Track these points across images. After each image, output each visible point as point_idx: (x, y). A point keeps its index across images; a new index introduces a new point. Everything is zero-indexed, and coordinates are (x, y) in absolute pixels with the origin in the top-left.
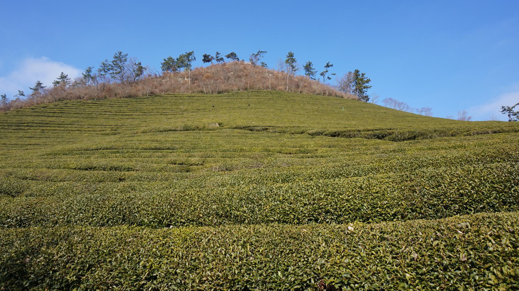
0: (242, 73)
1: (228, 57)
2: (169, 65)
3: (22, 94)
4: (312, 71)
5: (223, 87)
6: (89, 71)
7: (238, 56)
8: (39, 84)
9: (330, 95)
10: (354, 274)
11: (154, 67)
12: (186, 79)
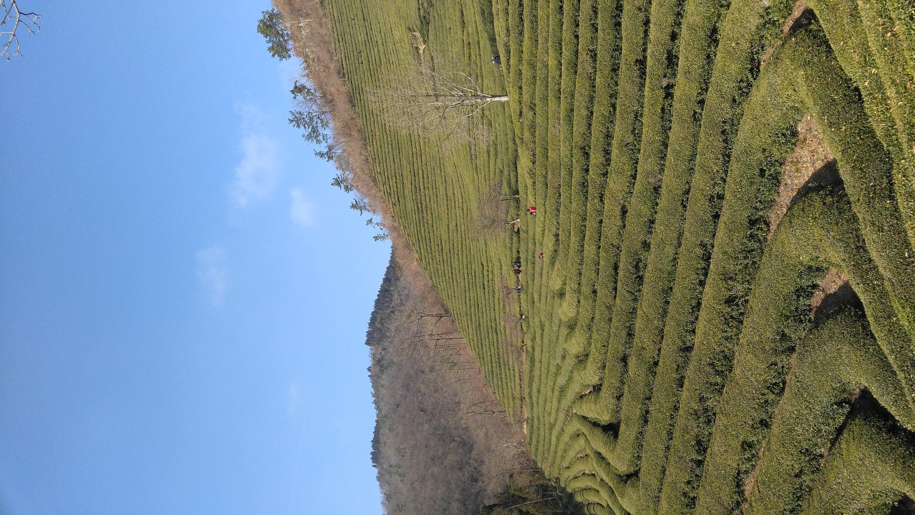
2: (279, 50)
3: (370, 221)
6: (322, 155)
8: (353, 206)
11: (292, 69)
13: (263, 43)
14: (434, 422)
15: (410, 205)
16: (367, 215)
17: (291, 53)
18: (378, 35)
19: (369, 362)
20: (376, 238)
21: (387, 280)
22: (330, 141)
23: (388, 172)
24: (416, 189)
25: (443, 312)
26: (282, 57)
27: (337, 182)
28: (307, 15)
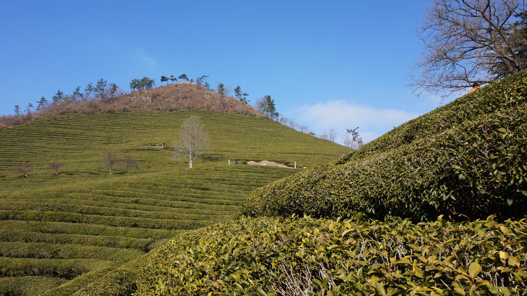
0: (188, 94)
1: (180, 78)
2: (135, 84)
3: (31, 106)
5: (173, 106)
6: (78, 89)
7: (188, 77)
8: (43, 99)
9: (246, 114)
10: (8, 125)
11: (125, 88)
12: (148, 98)
13: (140, 78)
15: (52, 130)
16: (36, 105)
17: (133, 90)
20: (17, 107)
22: (85, 96)
24: (65, 134)
26: (131, 84)
27: (59, 94)
28: (153, 101)
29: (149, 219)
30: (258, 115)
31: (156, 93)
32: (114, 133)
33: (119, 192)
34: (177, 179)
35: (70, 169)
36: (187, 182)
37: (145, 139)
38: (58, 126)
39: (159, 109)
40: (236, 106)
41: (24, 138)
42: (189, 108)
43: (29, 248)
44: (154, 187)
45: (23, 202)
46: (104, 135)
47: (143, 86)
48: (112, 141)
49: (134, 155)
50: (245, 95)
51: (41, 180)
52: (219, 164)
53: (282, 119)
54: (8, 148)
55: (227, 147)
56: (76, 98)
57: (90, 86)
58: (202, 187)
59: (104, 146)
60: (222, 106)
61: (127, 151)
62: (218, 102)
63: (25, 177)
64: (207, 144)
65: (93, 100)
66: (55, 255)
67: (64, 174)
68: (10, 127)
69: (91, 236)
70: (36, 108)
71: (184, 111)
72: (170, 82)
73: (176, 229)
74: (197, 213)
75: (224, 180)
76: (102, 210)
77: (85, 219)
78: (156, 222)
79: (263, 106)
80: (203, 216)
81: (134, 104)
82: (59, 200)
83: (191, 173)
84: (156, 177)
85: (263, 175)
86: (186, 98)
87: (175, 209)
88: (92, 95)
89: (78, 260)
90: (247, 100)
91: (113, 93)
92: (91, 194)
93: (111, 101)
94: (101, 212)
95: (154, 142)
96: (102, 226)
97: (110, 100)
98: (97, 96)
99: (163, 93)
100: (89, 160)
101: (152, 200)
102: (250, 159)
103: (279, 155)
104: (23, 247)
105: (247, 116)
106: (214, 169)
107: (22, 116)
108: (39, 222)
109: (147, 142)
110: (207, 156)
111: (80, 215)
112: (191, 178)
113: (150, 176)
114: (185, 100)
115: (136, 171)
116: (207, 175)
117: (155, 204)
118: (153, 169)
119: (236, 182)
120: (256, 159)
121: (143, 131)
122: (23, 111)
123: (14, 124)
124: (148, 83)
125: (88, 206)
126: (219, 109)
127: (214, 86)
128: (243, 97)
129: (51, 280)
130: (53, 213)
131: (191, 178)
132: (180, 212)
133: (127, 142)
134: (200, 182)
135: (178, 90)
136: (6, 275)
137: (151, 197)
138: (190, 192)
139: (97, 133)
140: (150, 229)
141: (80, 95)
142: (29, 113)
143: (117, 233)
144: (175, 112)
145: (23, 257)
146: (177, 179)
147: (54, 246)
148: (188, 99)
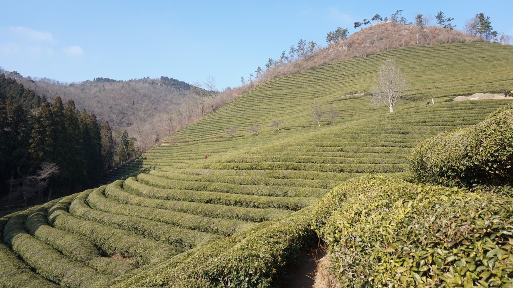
0: (384, 35)
1: (373, 19)
2: (331, 37)
3: (252, 76)
4: (443, 19)
5: (369, 50)
6: (283, 54)
7: (381, 16)
9: (453, 41)
10: (239, 94)
11: (322, 43)
12: (344, 48)
13: (334, 30)
14: (129, 109)
15: (269, 93)
16: (255, 74)
17: (329, 43)
18: (350, 80)
19: (152, 77)
20: (242, 78)
21: (183, 84)
22: (290, 58)
23: (277, 86)
24: (279, 95)
25: (214, 108)
27: (270, 61)
28: (349, 50)
29: (353, 165)
30: (468, 39)
31: (351, 41)
32: (318, 87)
33: (326, 143)
34: (377, 126)
35: (288, 125)
36: (386, 128)
37: (346, 89)
38: (273, 89)
39: (356, 57)
40: (440, 35)
41: (251, 103)
42: (386, 49)
43: (269, 189)
44: (356, 135)
45: (259, 156)
46: (310, 90)
47: (338, 37)
48: (317, 95)
49: (337, 106)
50: (449, 20)
51: (268, 136)
52: (423, 104)
53: (502, 38)
54: (242, 112)
55: (431, 84)
56: (283, 61)
57: (293, 49)
58: (402, 131)
59: (311, 101)
60: (423, 39)
61: (331, 102)
62: (418, 35)
63: (257, 135)
64: (406, 85)
65: (296, 60)
66: (285, 194)
67: (283, 130)
68: (240, 96)
69: (309, 180)
70: (256, 76)
71: (381, 53)
72: (363, 26)
73: (377, 173)
74: (397, 157)
75: (425, 122)
76: (315, 159)
77: (303, 167)
78: (359, 167)
79: (474, 27)
80: (402, 159)
81: (332, 56)
82: (283, 153)
83: (391, 117)
84: (358, 125)
85: (471, 112)
86: (382, 39)
87: (375, 154)
88: (296, 56)
89: (301, 198)
90: (452, 25)
91: (312, 50)
92: (305, 147)
93: (312, 58)
94: (314, 161)
95: (354, 90)
96: (316, 172)
97: (311, 57)
98: (299, 56)
99: (358, 39)
100: (300, 115)
101: (355, 147)
102: (459, 93)
103: (497, 84)
104: (265, 189)
105: (454, 44)
106: (415, 111)
107: (247, 85)
108: (272, 171)
109: (348, 92)
110: (409, 97)
111: (299, 164)
112: (391, 124)
113: (352, 125)
114: (381, 41)
115: (341, 120)
116: (408, 119)
117: (357, 151)
118: (356, 117)
119: (439, 123)
120: (467, 93)
121: (343, 81)
122: (247, 82)
123: (243, 93)
124: (343, 33)
125: (303, 157)
126: (420, 42)
127: (411, 19)
128: (447, 23)
129: (286, 211)
130: (280, 163)
131: (391, 124)
132: (380, 157)
133: (331, 94)
134: (400, 126)
135: (372, 33)
136: (258, 207)
137: (354, 145)
138: (390, 137)
139: (304, 90)
140: (354, 174)
141: (286, 58)
142: (252, 82)
143: (327, 177)
144: (372, 56)
145: (266, 195)
146: (377, 126)
147: (284, 188)
148: (384, 40)
